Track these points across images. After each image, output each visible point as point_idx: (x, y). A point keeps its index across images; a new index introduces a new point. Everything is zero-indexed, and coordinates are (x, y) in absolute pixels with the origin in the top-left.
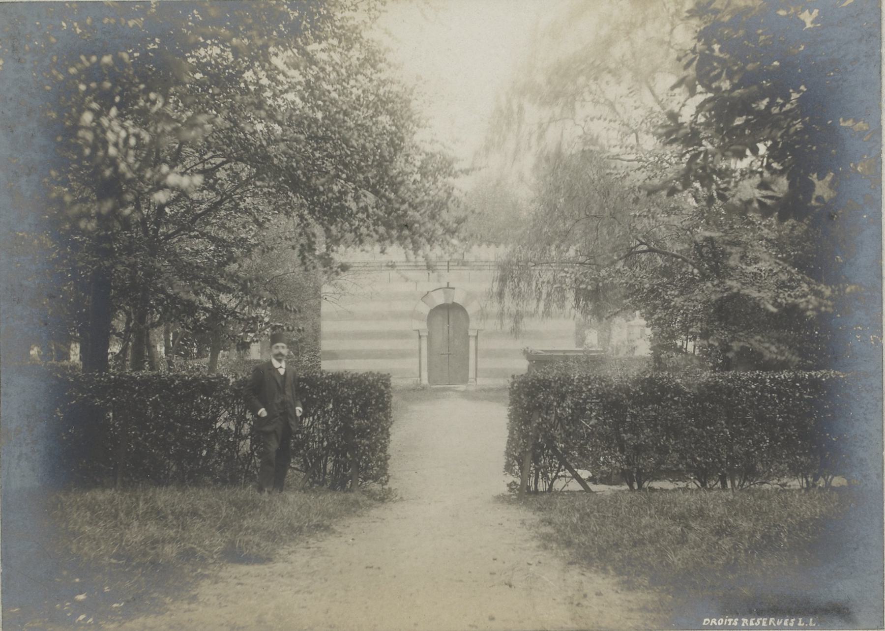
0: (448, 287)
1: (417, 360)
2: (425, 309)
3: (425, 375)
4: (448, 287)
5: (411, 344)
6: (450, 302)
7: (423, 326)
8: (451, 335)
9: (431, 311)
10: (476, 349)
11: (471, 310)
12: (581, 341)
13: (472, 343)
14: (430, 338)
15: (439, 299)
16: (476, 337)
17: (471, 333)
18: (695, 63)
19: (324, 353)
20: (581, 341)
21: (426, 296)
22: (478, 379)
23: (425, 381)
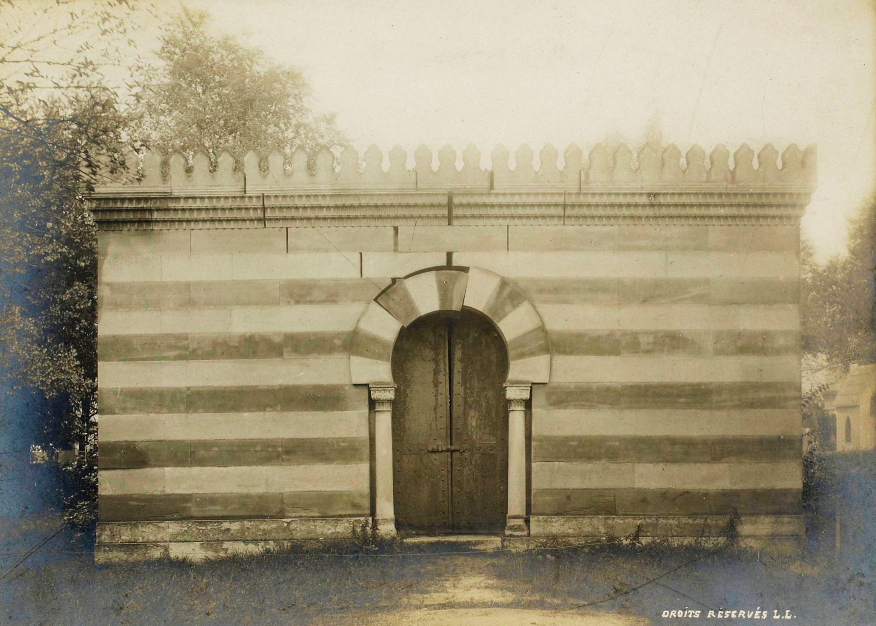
0: (449, 266)
1: (365, 467)
2: (386, 327)
3: (386, 509)
4: (449, 266)
5: (349, 423)
6: (456, 306)
7: (380, 371)
8: (458, 400)
9: (404, 334)
10: (528, 437)
11: (512, 326)
12: (517, 383)
13: (517, 419)
14: (398, 408)
15: (426, 299)
16: (528, 404)
17: (512, 393)
18: (439, 598)
19: (111, 448)
20: (517, 383)
21: (388, 293)
22: (533, 519)
23: (387, 529)
